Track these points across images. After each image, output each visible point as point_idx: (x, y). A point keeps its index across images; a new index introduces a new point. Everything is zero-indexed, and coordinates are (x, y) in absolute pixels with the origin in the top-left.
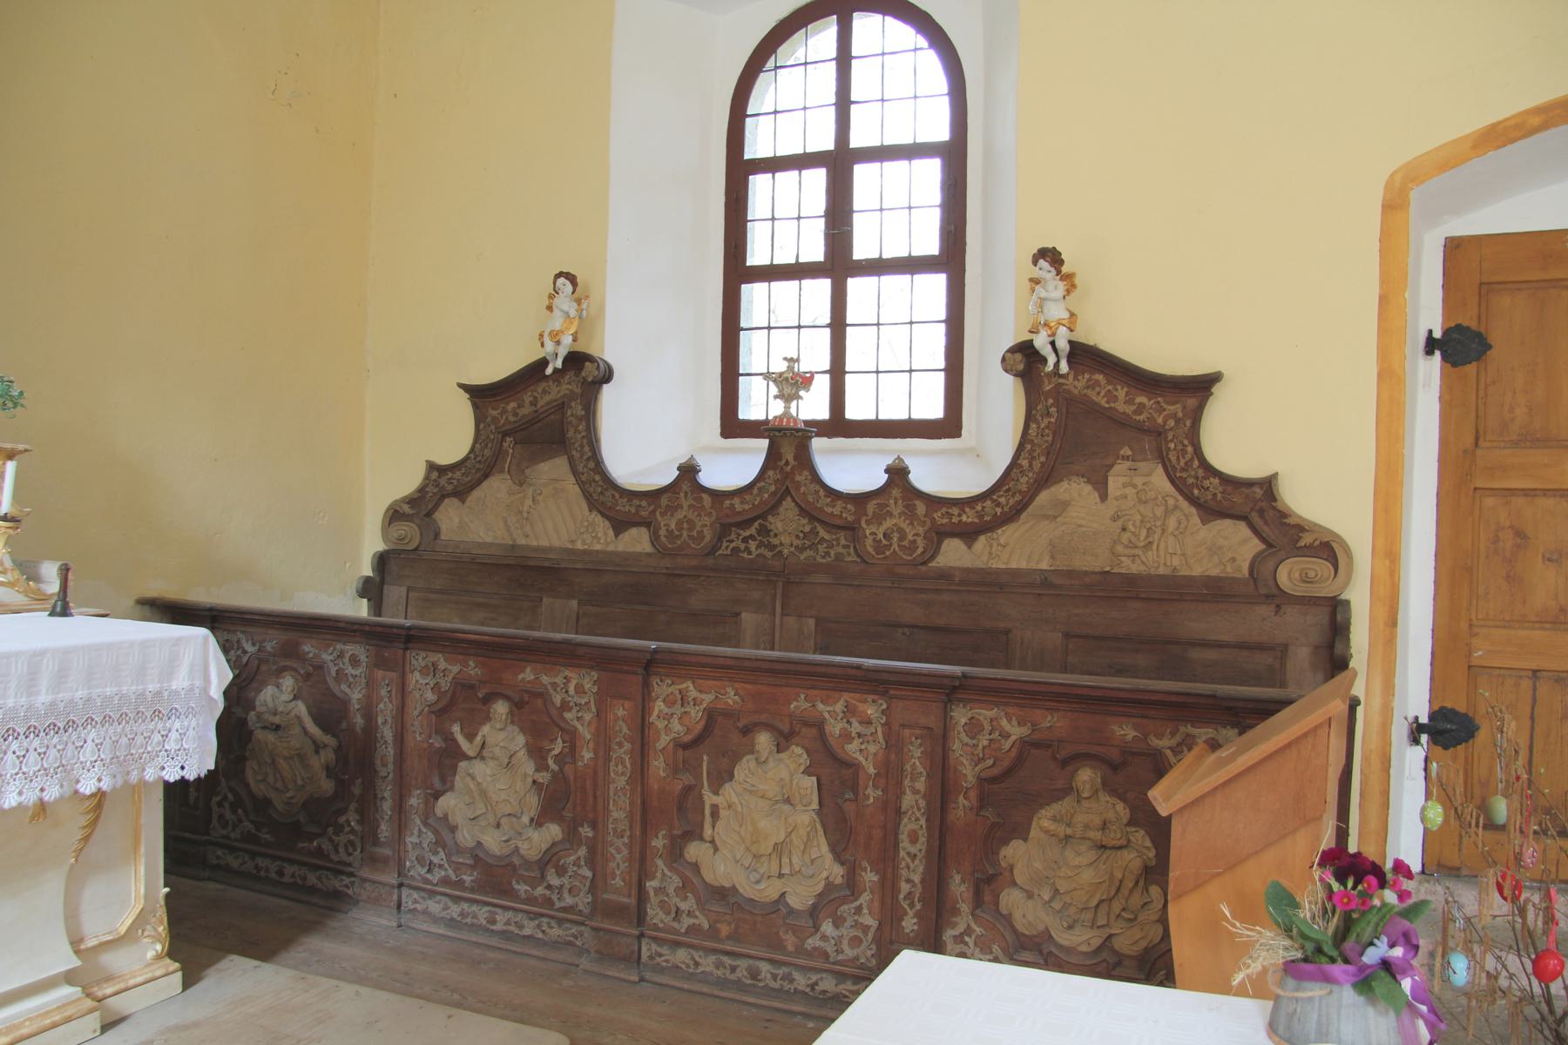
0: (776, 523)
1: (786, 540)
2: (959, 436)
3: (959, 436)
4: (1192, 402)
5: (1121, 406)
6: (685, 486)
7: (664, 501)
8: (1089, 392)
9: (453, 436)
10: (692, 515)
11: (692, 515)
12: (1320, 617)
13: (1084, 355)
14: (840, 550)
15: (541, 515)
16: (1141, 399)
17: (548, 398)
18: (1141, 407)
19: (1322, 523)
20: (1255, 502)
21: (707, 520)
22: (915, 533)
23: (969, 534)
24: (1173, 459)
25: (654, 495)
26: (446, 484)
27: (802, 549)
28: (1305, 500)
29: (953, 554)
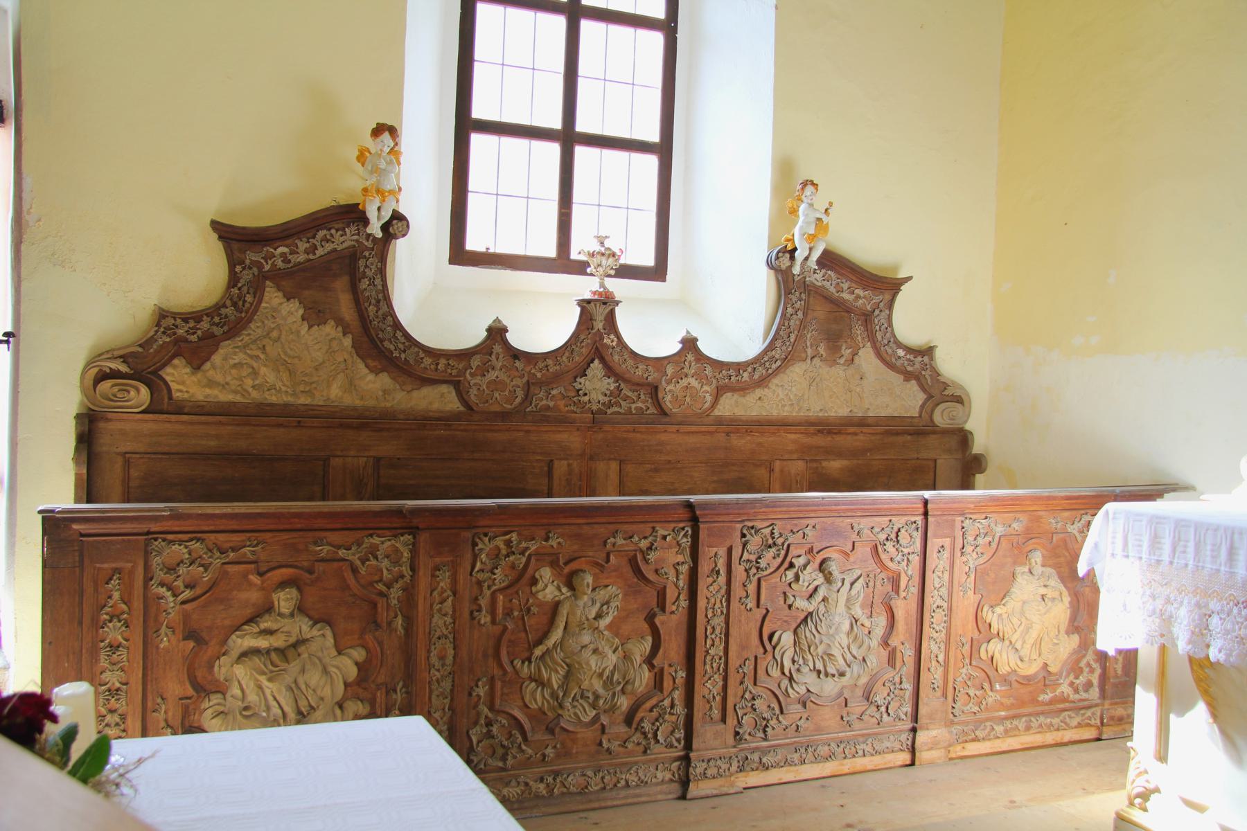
0: (584, 383)
1: (594, 396)
2: (664, 280)
3: (664, 280)
4: (888, 297)
5: (846, 296)
6: (498, 348)
7: (476, 362)
8: (825, 283)
9: (199, 275)
10: (503, 376)
11: (503, 376)
12: (953, 442)
13: (830, 260)
14: (640, 405)
15: (295, 360)
16: (859, 292)
17: (329, 247)
18: (858, 297)
19: (956, 380)
20: (918, 364)
21: (518, 382)
22: (707, 391)
23: (742, 389)
24: (879, 338)
25: (464, 355)
26: (181, 336)
27: (610, 405)
28: (949, 364)
29: (729, 406)
